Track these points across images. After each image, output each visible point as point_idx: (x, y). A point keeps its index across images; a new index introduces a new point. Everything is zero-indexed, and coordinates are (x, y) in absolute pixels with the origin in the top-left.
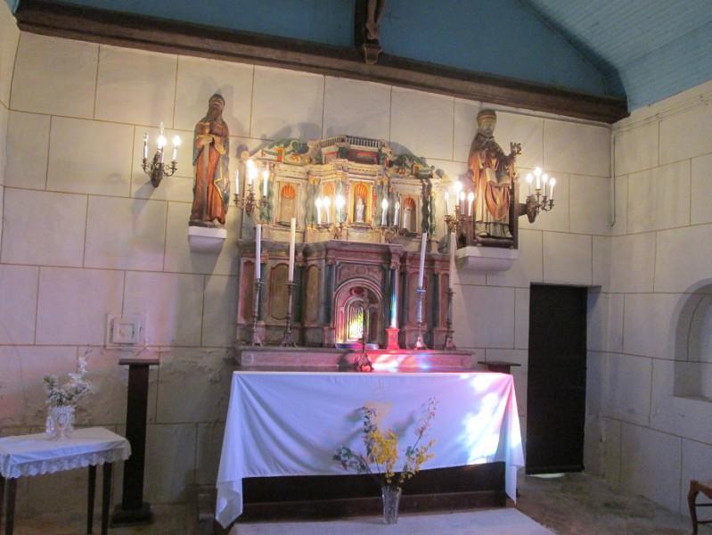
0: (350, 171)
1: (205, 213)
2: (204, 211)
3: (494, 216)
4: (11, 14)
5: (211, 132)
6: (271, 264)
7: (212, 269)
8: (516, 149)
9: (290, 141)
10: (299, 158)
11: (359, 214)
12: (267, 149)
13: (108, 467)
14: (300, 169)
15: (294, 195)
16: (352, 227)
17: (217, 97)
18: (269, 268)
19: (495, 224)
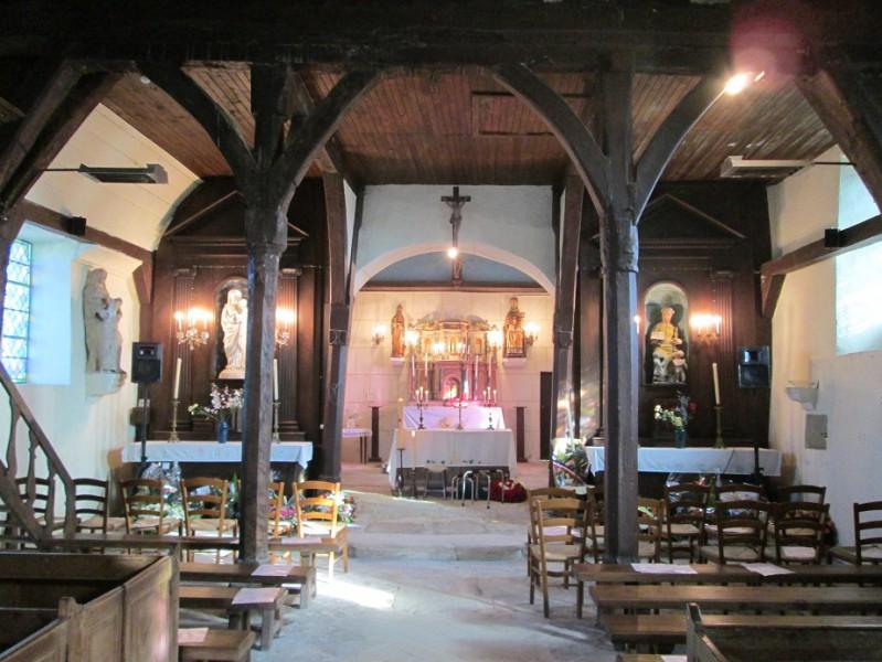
2: (396, 352)
13: (366, 438)
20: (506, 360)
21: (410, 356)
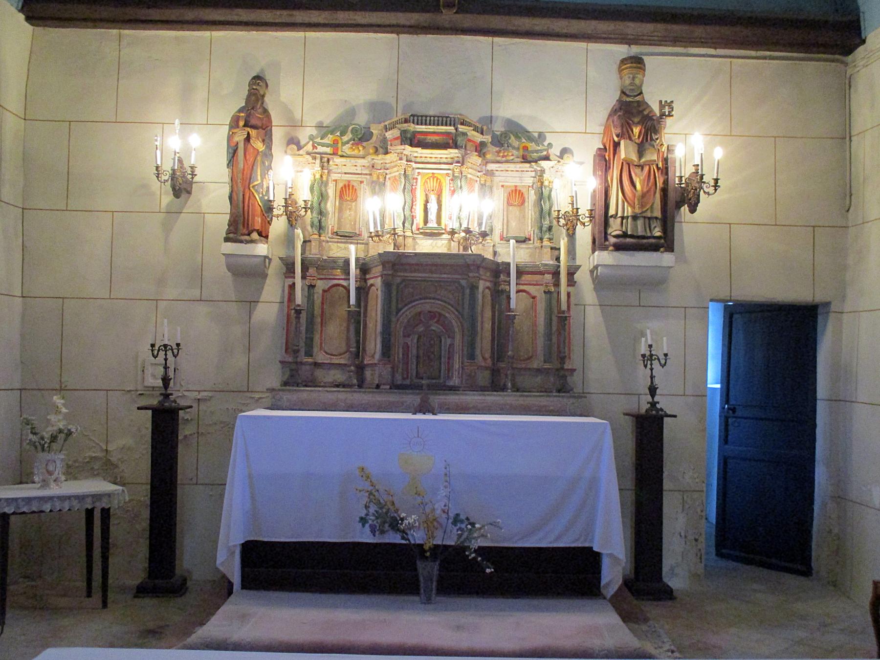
0: (418, 160)
1: (241, 227)
3: (633, 207)
4: (16, 11)
5: (245, 125)
6: (321, 285)
7: (259, 297)
8: (667, 110)
9: (347, 127)
10: (361, 148)
11: (432, 216)
12: (318, 140)
14: (361, 162)
15: (357, 197)
16: (421, 233)
17: (258, 79)
18: (321, 292)
19: (635, 218)
20: (606, 257)
21: (289, 240)
